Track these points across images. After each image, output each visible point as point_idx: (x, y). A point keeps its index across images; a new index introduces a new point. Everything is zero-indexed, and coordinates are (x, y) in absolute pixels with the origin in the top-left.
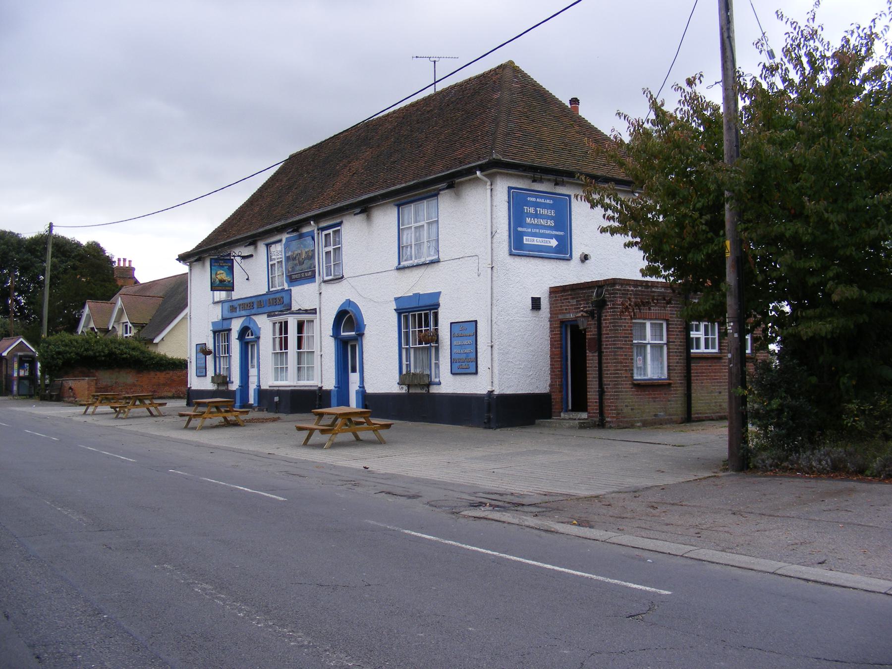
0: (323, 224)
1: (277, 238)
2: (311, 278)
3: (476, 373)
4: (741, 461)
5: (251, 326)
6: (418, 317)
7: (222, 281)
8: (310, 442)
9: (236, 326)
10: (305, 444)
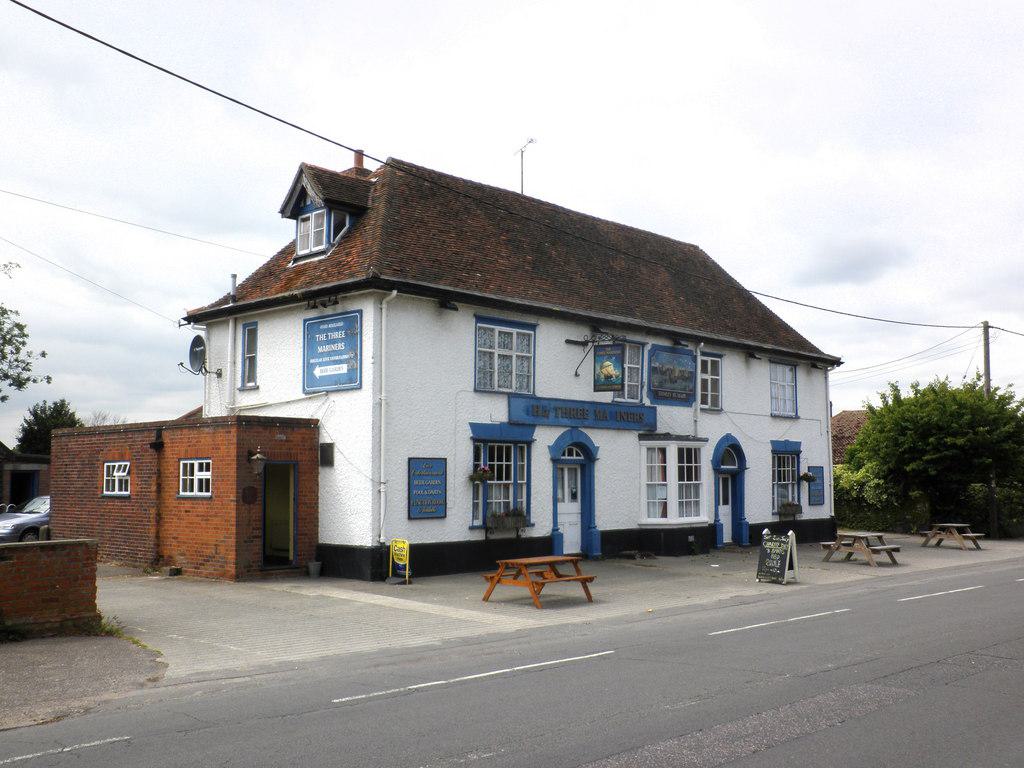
1: (638, 338)
7: (608, 377)
8: (492, 597)
10: (486, 599)
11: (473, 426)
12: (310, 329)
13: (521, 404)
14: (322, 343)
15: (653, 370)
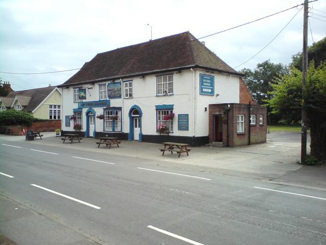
0: (124, 80)
1: (104, 83)
2: (120, 97)
3: (188, 130)
4: (306, 161)
5: (92, 111)
6: (166, 113)
7: (82, 96)
9: (85, 110)
10: (99, 147)
11: (156, 106)
12: (202, 77)
13: (80, 104)
14: (205, 82)
15: (109, 90)
